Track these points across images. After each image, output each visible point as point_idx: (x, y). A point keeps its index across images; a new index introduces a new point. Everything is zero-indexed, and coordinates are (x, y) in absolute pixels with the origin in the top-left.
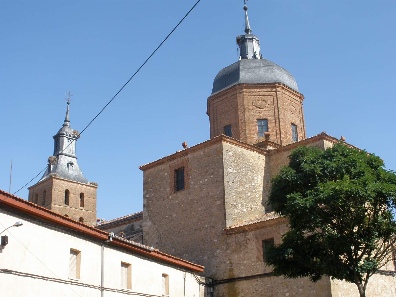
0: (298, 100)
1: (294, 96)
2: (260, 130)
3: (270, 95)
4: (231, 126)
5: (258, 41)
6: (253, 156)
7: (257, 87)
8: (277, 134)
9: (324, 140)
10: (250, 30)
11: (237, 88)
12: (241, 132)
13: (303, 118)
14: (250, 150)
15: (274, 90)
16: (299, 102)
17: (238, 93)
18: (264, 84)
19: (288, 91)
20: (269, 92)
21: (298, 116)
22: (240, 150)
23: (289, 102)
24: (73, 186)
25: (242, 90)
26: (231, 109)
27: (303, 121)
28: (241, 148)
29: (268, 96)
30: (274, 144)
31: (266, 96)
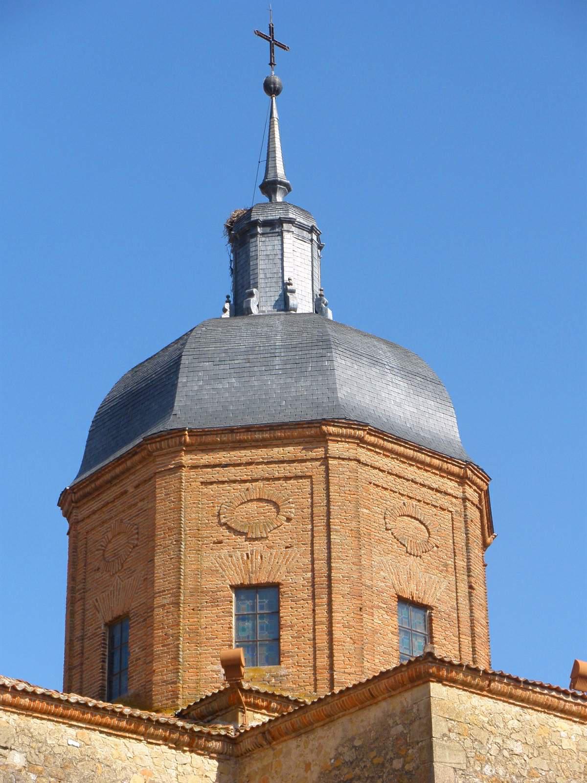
0: (450, 491)
1: (427, 471)
2: (243, 635)
3: (297, 477)
4: (130, 619)
5: (311, 230)
6: (148, 762)
7: (240, 441)
8: (315, 651)
9: (437, 689)
10: (281, 183)
11: (157, 450)
12: (158, 648)
13: (469, 570)
14: (127, 735)
15: (319, 452)
16: (456, 498)
17: (158, 472)
18: (271, 427)
19: (391, 451)
20: (293, 461)
21: (446, 565)
22: (70, 742)
23: (397, 502)
25: (177, 460)
26: (135, 546)
27: (471, 587)
28: (79, 731)
29: (290, 478)
30: (276, 701)
31: (279, 479)
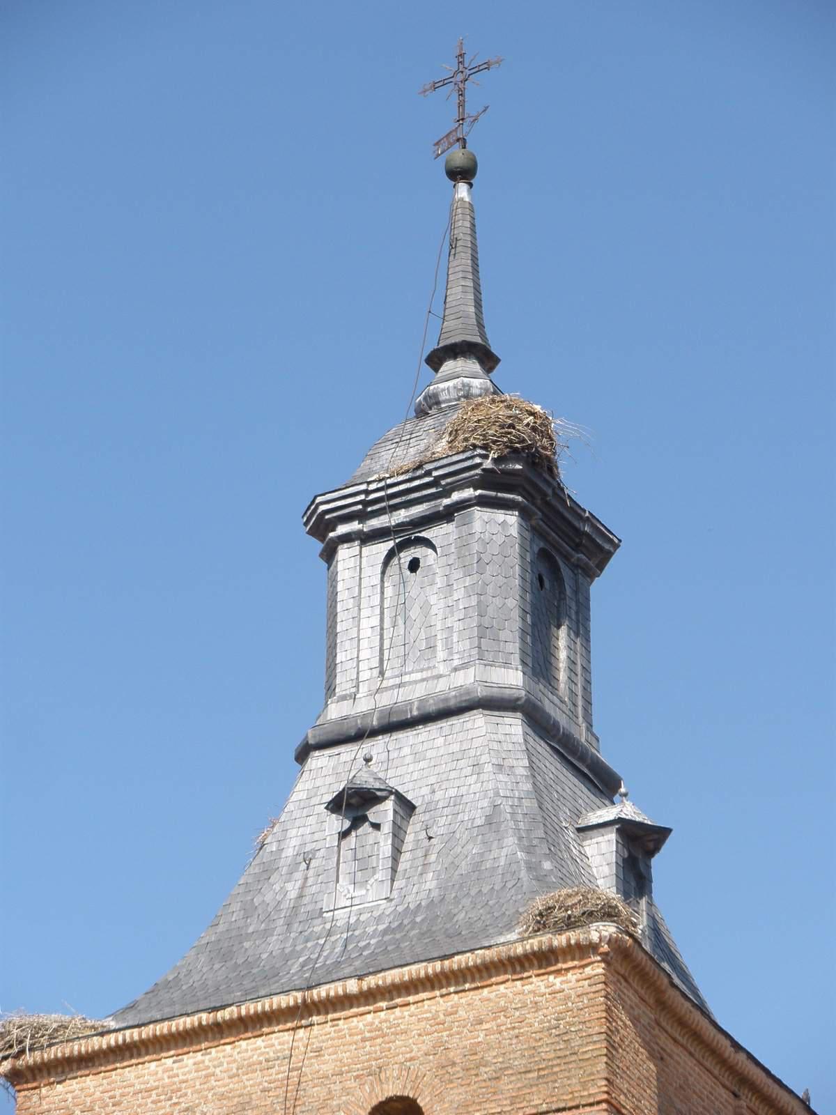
24: (268, 1064)
